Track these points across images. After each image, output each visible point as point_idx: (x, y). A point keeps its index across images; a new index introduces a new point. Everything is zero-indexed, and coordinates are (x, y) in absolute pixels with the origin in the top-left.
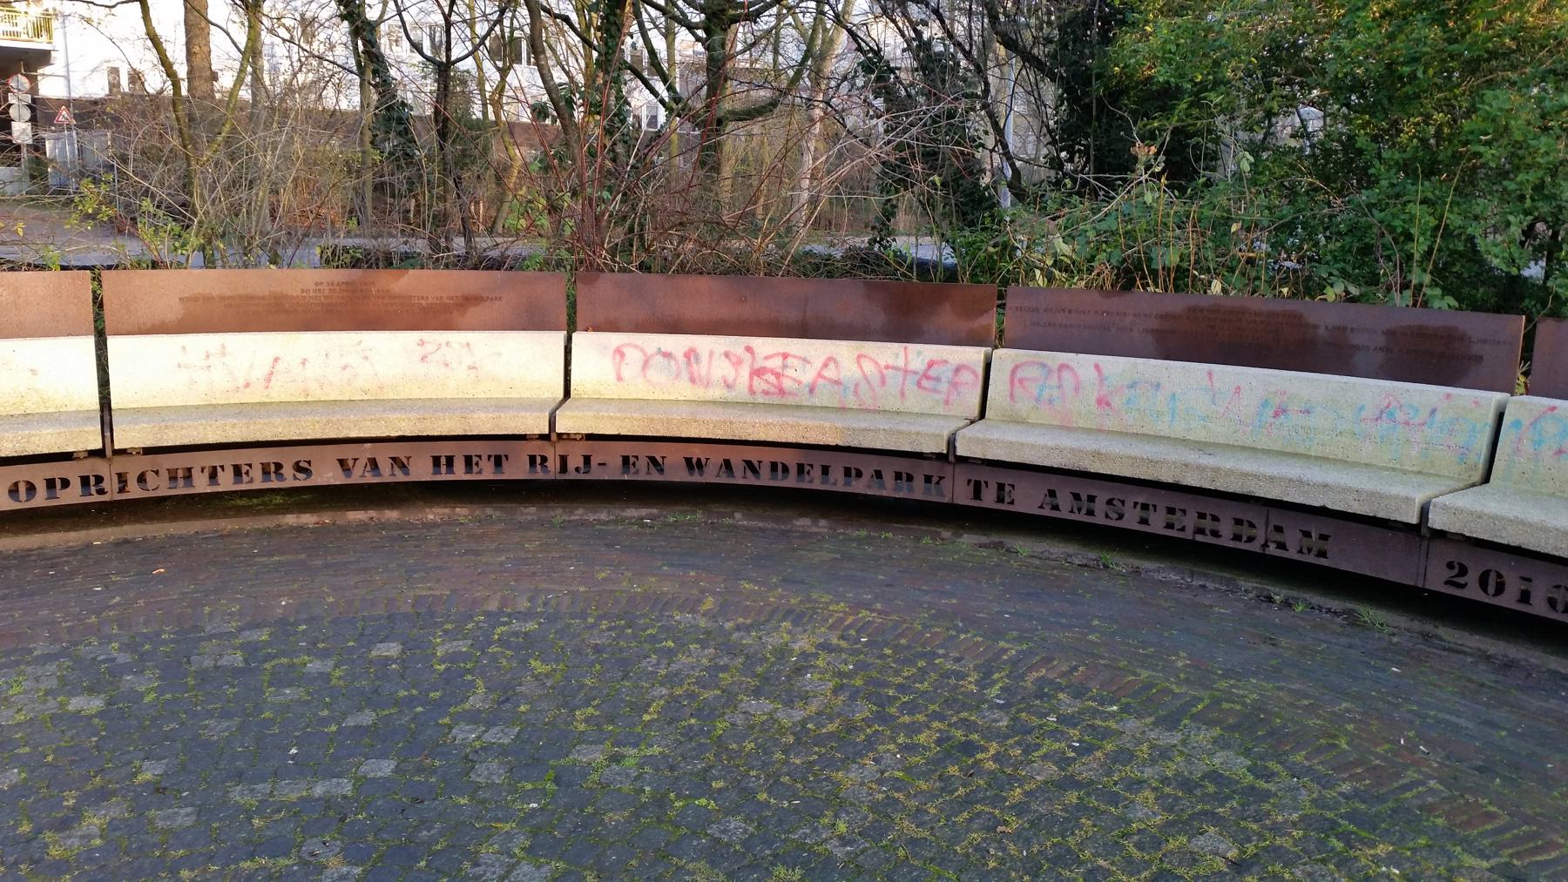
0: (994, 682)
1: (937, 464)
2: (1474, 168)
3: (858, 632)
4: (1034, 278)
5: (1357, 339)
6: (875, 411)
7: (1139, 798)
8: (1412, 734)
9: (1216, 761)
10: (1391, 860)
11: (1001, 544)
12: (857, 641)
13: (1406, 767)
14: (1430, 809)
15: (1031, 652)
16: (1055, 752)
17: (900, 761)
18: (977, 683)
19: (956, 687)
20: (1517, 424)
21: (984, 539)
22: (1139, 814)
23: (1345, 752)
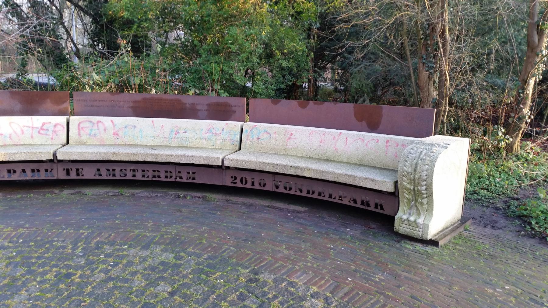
0: (79, 247)
1: (49, 164)
2: (230, 52)
3: (18, 238)
4: (86, 89)
5: (198, 107)
6: (20, 145)
7: (136, 278)
8: (225, 233)
9: (163, 257)
10: (221, 277)
11: (80, 192)
12: (17, 242)
13: (224, 244)
14: (230, 257)
15: (93, 232)
16: (104, 268)
17: (38, 288)
18: (71, 249)
19: (63, 252)
20: (247, 131)
21: (72, 191)
22: (136, 284)
23: (205, 244)
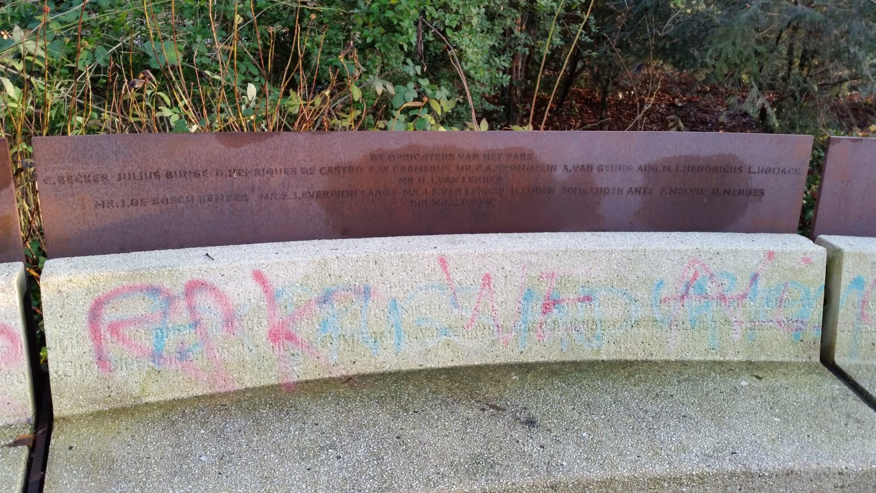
5: (604, 181)
20: (858, 282)
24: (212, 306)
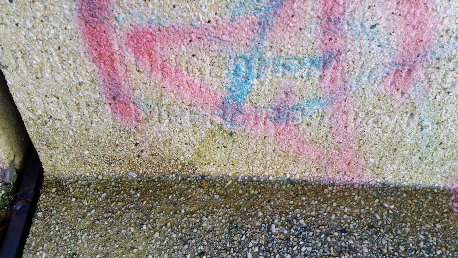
24: (383, 23)
